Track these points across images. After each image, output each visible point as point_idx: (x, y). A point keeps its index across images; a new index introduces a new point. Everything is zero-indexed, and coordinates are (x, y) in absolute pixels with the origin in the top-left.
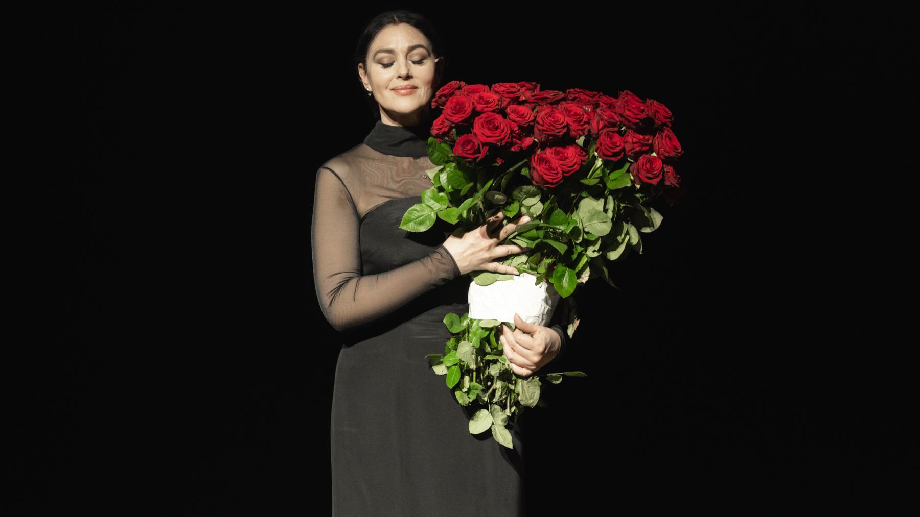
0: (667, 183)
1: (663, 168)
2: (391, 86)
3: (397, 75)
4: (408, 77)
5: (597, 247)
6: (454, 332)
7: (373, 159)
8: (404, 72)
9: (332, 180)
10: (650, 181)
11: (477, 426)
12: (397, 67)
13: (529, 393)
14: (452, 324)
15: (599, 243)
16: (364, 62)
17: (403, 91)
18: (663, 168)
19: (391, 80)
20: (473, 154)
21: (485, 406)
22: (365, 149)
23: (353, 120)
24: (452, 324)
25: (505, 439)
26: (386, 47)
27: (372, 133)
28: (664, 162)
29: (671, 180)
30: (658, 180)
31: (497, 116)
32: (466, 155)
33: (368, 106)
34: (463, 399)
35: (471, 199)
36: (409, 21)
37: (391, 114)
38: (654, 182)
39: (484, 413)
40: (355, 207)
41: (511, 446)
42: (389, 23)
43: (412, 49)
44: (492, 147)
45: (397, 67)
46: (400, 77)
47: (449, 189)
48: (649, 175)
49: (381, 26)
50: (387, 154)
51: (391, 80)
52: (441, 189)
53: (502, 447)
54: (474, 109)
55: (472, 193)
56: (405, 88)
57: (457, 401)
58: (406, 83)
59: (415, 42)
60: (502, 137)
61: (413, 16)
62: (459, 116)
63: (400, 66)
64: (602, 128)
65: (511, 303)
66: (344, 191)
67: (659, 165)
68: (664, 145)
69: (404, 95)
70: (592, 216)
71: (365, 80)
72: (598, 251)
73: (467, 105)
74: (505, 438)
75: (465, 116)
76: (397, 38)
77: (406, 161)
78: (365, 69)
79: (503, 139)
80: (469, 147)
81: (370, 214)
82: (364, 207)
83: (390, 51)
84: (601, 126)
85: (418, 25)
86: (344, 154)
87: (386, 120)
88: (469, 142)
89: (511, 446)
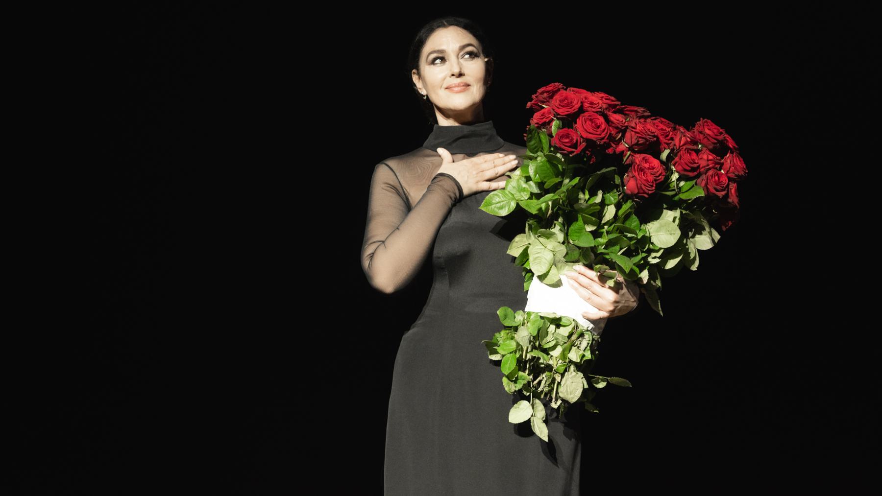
0: (730, 200)
1: (728, 185)
2: (445, 85)
3: (450, 74)
4: (461, 75)
5: (659, 254)
6: (506, 324)
8: (456, 71)
10: (717, 193)
11: (520, 413)
12: (450, 70)
13: (573, 387)
14: (506, 316)
15: (662, 251)
16: (417, 67)
17: (456, 89)
18: (728, 185)
19: (444, 79)
20: (570, 147)
21: (527, 399)
23: (412, 126)
24: (506, 316)
25: (541, 432)
26: (437, 49)
28: (730, 179)
29: (733, 199)
30: (723, 193)
31: (599, 117)
32: (563, 147)
35: (552, 195)
36: (458, 24)
37: (443, 111)
38: (721, 194)
39: (524, 404)
40: (424, 196)
41: (546, 439)
42: (439, 27)
43: (463, 47)
44: (590, 143)
45: (450, 70)
47: (537, 178)
48: (718, 188)
49: (431, 31)
50: (471, 154)
51: (444, 79)
52: (528, 179)
54: (582, 107)
55: (555, 188)
56: (459, 86)
58: (459, 80)
59: (466, 42)
60: (603, 136)
61: (461, 20)
62: (565, 109)
63: (453, 65)
65: (567, 297)
67: (725, 180)
68: (733, 164)
69: (460, 92)
70: (663, 231)
71: (419, 84)
72: (659, 258)
73: (576, 102)
74: (541, 431)
75: (572, 111)
76: (448, 39)
78: (419, 74)
79: (602, 139)
80: (567, 140)
83: (442, 51)
84: (682, 143)
85: (466, 27)
88: (567, 136)
89: (546, 439)
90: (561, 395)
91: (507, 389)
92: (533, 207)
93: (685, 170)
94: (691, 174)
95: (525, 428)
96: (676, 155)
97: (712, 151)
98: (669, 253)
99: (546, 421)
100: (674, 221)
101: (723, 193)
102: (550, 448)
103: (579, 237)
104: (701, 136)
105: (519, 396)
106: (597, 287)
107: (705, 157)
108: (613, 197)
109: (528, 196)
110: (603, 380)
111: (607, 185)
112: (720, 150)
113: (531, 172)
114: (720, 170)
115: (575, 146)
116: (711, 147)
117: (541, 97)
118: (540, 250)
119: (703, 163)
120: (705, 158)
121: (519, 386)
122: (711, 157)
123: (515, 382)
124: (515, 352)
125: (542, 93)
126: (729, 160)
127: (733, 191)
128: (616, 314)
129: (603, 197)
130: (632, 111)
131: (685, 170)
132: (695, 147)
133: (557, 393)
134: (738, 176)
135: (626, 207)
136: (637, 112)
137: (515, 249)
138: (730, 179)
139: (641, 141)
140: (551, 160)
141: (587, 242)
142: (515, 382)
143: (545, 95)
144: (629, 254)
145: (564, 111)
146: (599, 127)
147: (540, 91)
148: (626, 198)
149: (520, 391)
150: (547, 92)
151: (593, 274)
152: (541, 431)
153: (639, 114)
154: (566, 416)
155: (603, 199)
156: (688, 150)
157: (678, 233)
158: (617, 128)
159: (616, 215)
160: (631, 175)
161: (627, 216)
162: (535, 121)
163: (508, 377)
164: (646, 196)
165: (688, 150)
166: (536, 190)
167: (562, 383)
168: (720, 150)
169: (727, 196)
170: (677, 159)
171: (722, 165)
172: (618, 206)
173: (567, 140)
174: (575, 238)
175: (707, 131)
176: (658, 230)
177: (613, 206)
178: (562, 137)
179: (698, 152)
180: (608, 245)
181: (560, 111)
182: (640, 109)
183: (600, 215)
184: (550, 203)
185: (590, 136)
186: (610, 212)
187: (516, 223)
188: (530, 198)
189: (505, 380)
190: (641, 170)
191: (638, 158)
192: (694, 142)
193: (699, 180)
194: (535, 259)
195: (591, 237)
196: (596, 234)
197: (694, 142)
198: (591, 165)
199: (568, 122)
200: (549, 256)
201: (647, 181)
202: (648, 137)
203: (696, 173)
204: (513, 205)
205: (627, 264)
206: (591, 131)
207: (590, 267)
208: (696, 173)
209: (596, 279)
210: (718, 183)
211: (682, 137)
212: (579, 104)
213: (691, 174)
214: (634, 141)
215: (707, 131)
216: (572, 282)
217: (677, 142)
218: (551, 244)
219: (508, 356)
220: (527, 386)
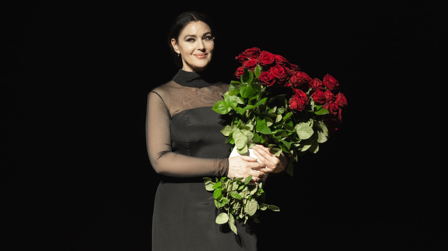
7: (176, 88)
8: (202, 47)
9: (155, 100)
11: (222, 219)
13: (252, 208)
21: (226, 212)
22: (173, 83)
27: (177, 75)
30: (336, 113)
33: (177, 60)
34: (218, 205)
39: (224, 215)
41: (236, 233)
46: (199, 50)
53: (235, 234)
57: (215, 205)
64: (318, 87)
65: (249, 160)
66: (162, 106)
70: (304, 131)
71: (176, 47)
72: (299, 143)
73: (271, 59)
77: (194, 89)
80: (266, 78)
81: (176, 116)
82: (173, 111)
84: (317, 86)
86: (163, 86)
87: (186, 68)
89: (236, 233)
90: (245, 211)
91: (216, 206)
92: (241, 111)
93: (319, 100)
94: (321, 102)
95: (225, 227)
96: (315, 91)
97: (332, 91)
98: (304, 142)
99: (235, 224)
100: (310, 126)
101: (336, 113)
102: (238, 237)
103: (262, 129)
104: (328, 83)
105: (223, 210)
106: (268, 156)
107: (328, 94)
108: (281, 111)
109: (236, 105)
110: (265, 206)
111: (280, 104)
112: (335, 92)
113: (241, 93)
114: (335, 101)
115: (271, 82)
116: (331, 89)
117: (248, 54)
118: (239, 136)
119: (327, 97)
120: (328, 95)
121: (223, 205)
122: (331, 94)
123: (221, 202)
124: (221, 188)
125: (250, 51)
126: (340, 96)
127: (340, 112)
128: (276, 172)
129: (277, 109)
130: (292, 66)
131: (319, 100)
132: (323, 88)
133: (243, 210)
134: (344, 105)
135: (288, 115)
136: (295, 67)
137: (226, 132)
138: (340, 107)
139: (300, 81)
140: (255, 86)
141: (267, 131)
142: (221, 202)
143: (251, 53)
144: (287, 140)
145: (265, 62)
146: (281, 72)
147: (247, 50)
148: (289, 110)
149: (223, 207)
150: (253, 51)
151: (267, 149)
152: (234, 229)
153: (296, 69)
154: (254, 224)
155: (277, 111)
156: (321, 90)
157: (312, 132)
158: (288, 74)
159: (282, 119)
160: (294, 99)
161: (288, 121)
162: (245, 65)
163: (217, 200)
164: (301, 111)
165: (321, 90)
166: (241, 102)
167: (247, 205)
168: (335, 92)
169: (337, 115)
170: (315, 93)
171: (336, 99)
172: (283, 115)
173: (266, 78)
174: (259, 129)
175: (331, 81)
176: (301, 130)
177: (281, 115)
178: (264, 75)
179: (324, 91)
180: (277, 135)
181: (264, 62)
182: (297, 66)
183: (274, 119)
184: (248, 111)
185: (277, 76)
186: (279, 118)
187: (228, 119)
188: (237, 106)
189: (215, 201)
190: (300, 97)
191: (297, 90)
192: (323, 86)
193: (324, 106)
194: (238, 140)
195: (269, 130)
196: (272, 128)
197: (323, 86)
198: (277, 93)
199: (265, 68)
200: (245, 139)
201: (302, 103)
202: (303, 80)
203: (323, 102)
204: (229, 110)
205: (288, 145)
206: (278, 74)
207: (265, 146)
208: (323, 102)
209: (268, 152)
210: (335, 107)
211: (316, 83)
212: (273, 60)
213: (321, 102)
214: (296, 81)
215: (331, 81)
216: (255, 152)
217: (314, 85)
218: (246, 132)
219: (218, 189)
220: (227, 206)
